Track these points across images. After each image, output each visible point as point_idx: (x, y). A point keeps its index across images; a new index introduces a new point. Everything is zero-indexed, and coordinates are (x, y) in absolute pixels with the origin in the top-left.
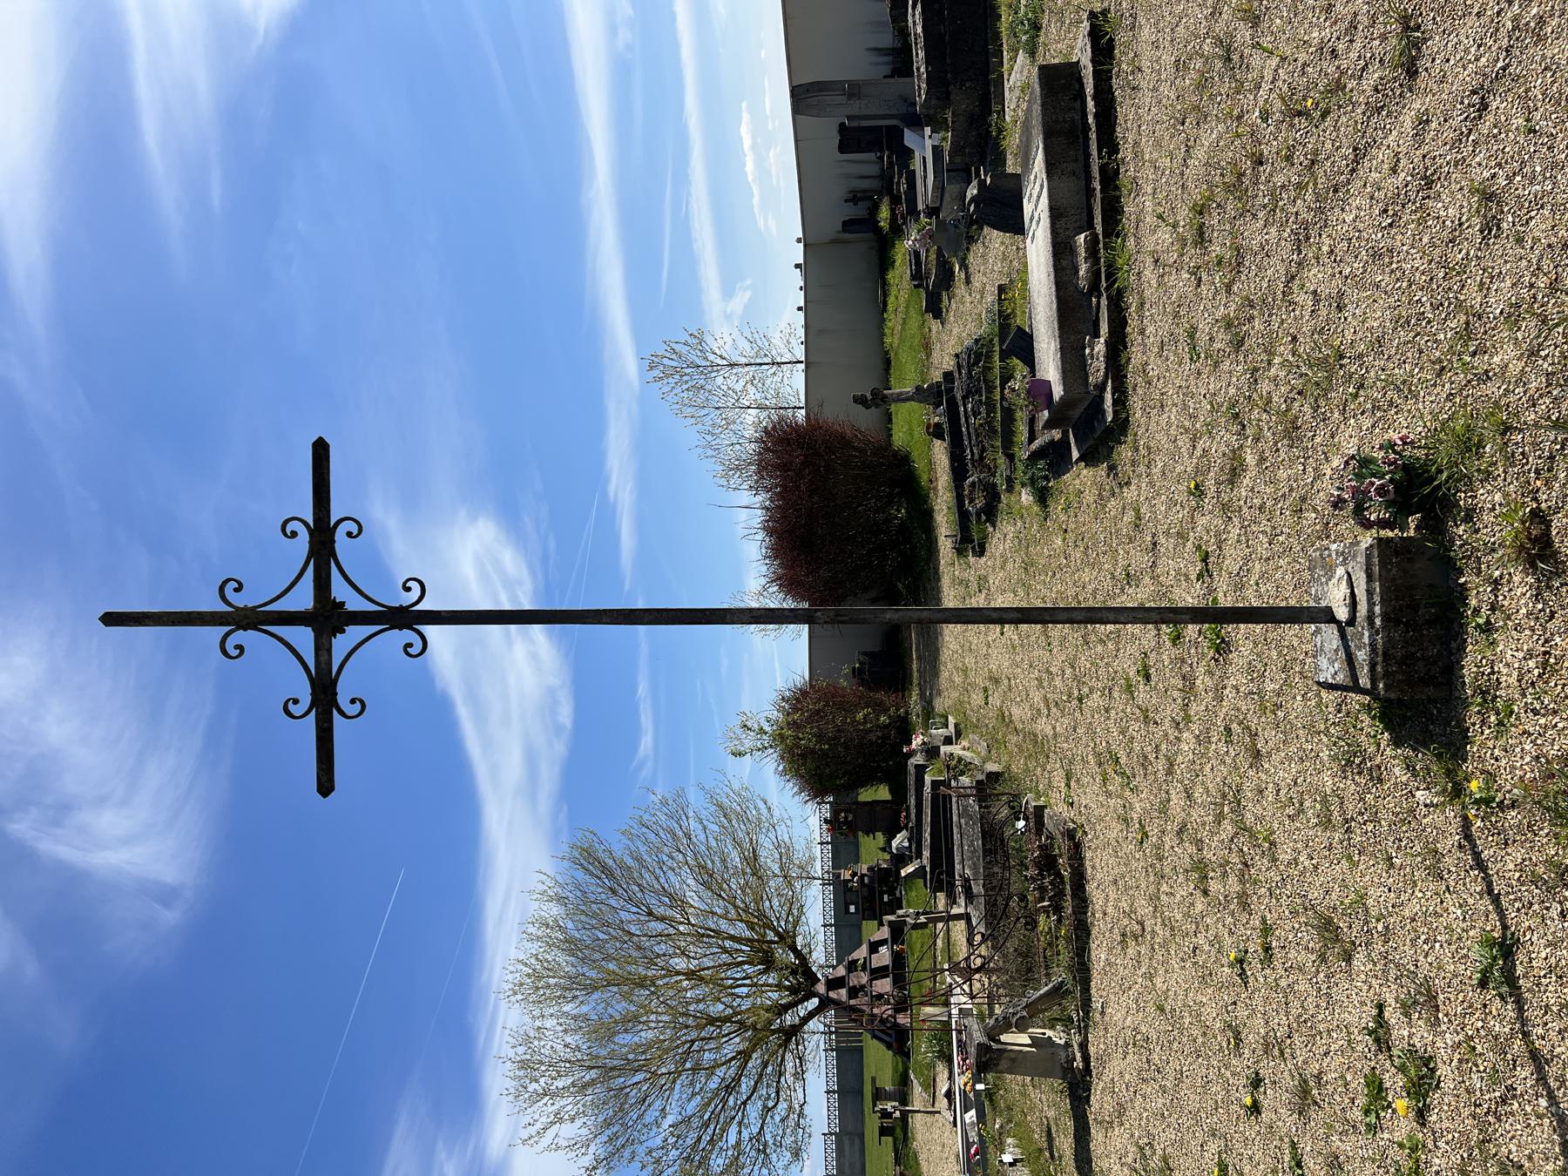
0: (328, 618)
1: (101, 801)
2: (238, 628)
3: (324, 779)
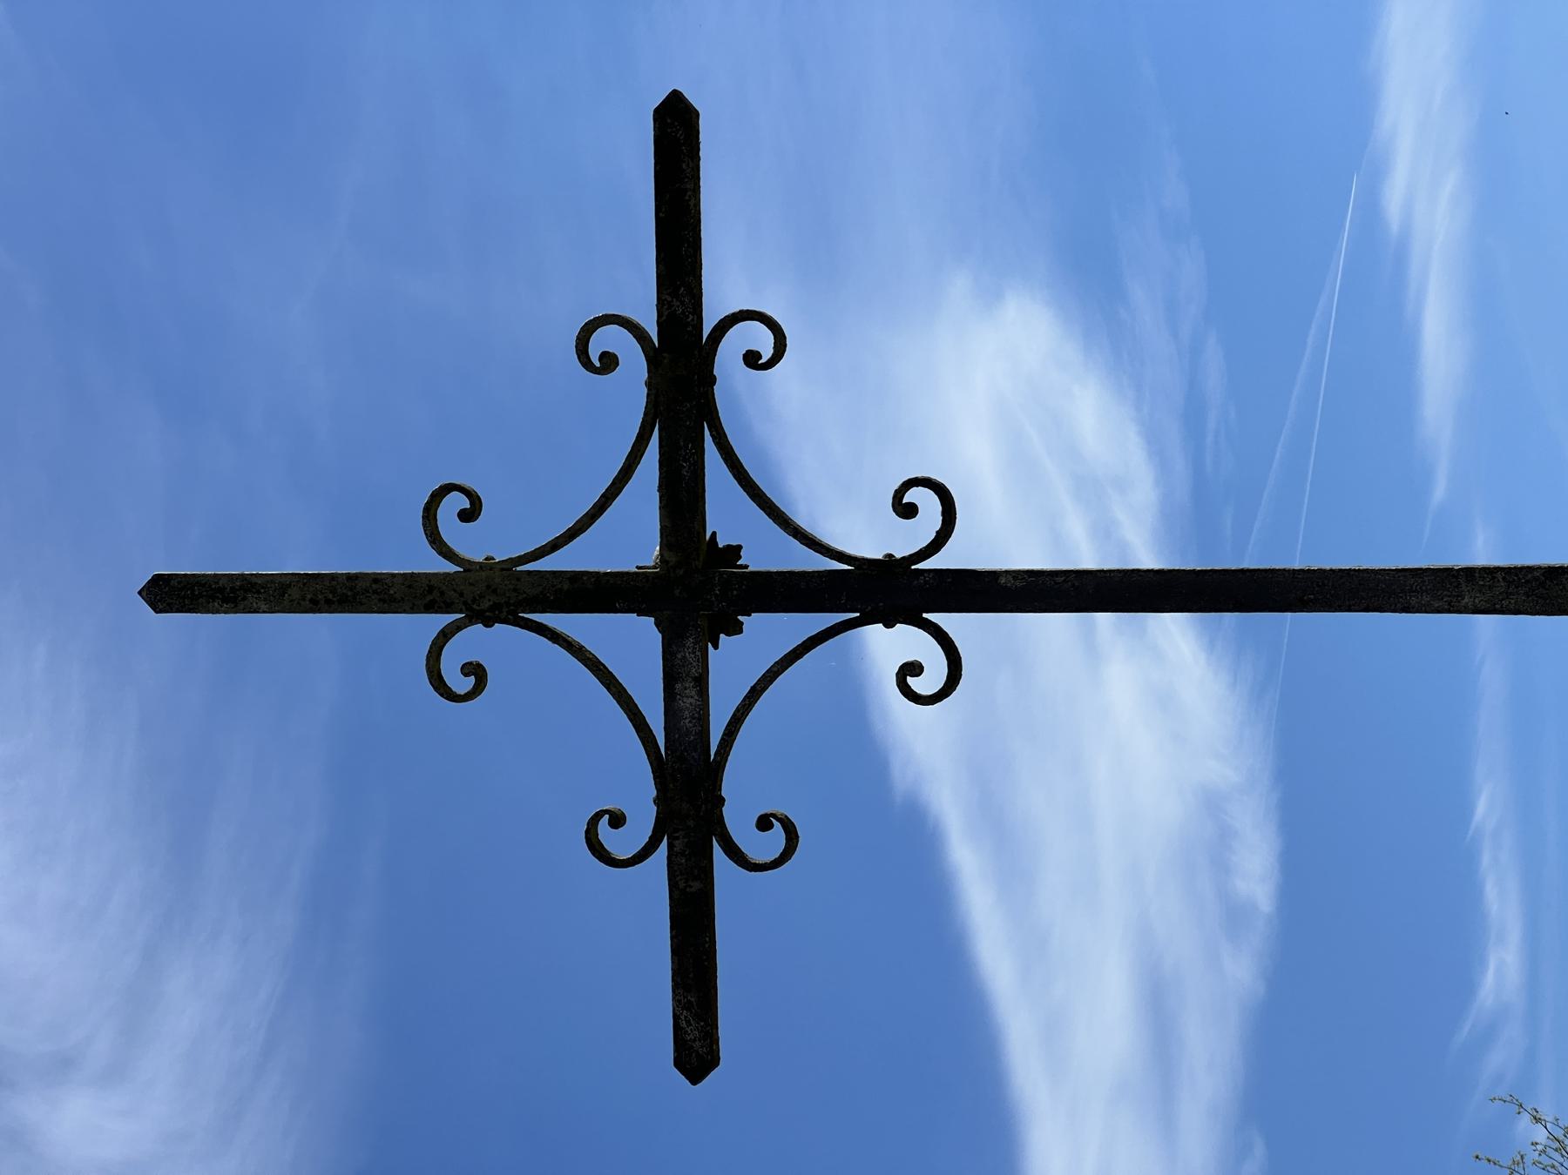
0: (697, 591)
1: (61, 1067)
2: (471, 619)
3: (692, 1033)
